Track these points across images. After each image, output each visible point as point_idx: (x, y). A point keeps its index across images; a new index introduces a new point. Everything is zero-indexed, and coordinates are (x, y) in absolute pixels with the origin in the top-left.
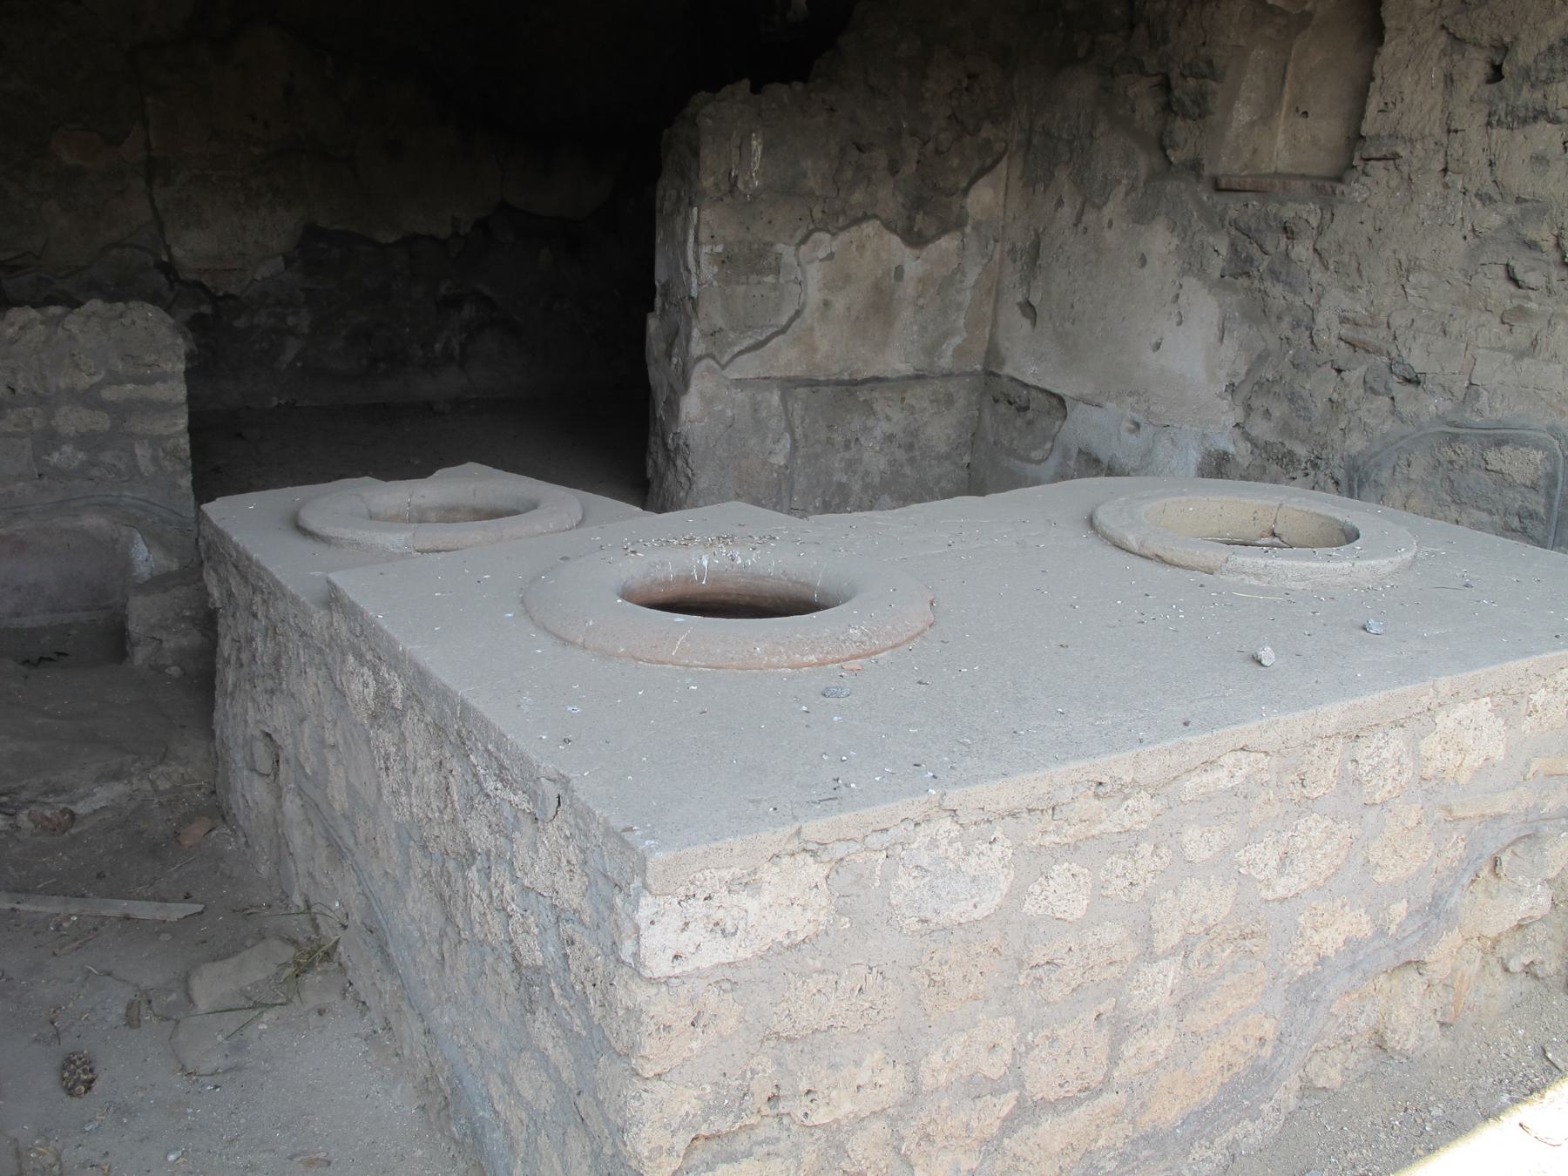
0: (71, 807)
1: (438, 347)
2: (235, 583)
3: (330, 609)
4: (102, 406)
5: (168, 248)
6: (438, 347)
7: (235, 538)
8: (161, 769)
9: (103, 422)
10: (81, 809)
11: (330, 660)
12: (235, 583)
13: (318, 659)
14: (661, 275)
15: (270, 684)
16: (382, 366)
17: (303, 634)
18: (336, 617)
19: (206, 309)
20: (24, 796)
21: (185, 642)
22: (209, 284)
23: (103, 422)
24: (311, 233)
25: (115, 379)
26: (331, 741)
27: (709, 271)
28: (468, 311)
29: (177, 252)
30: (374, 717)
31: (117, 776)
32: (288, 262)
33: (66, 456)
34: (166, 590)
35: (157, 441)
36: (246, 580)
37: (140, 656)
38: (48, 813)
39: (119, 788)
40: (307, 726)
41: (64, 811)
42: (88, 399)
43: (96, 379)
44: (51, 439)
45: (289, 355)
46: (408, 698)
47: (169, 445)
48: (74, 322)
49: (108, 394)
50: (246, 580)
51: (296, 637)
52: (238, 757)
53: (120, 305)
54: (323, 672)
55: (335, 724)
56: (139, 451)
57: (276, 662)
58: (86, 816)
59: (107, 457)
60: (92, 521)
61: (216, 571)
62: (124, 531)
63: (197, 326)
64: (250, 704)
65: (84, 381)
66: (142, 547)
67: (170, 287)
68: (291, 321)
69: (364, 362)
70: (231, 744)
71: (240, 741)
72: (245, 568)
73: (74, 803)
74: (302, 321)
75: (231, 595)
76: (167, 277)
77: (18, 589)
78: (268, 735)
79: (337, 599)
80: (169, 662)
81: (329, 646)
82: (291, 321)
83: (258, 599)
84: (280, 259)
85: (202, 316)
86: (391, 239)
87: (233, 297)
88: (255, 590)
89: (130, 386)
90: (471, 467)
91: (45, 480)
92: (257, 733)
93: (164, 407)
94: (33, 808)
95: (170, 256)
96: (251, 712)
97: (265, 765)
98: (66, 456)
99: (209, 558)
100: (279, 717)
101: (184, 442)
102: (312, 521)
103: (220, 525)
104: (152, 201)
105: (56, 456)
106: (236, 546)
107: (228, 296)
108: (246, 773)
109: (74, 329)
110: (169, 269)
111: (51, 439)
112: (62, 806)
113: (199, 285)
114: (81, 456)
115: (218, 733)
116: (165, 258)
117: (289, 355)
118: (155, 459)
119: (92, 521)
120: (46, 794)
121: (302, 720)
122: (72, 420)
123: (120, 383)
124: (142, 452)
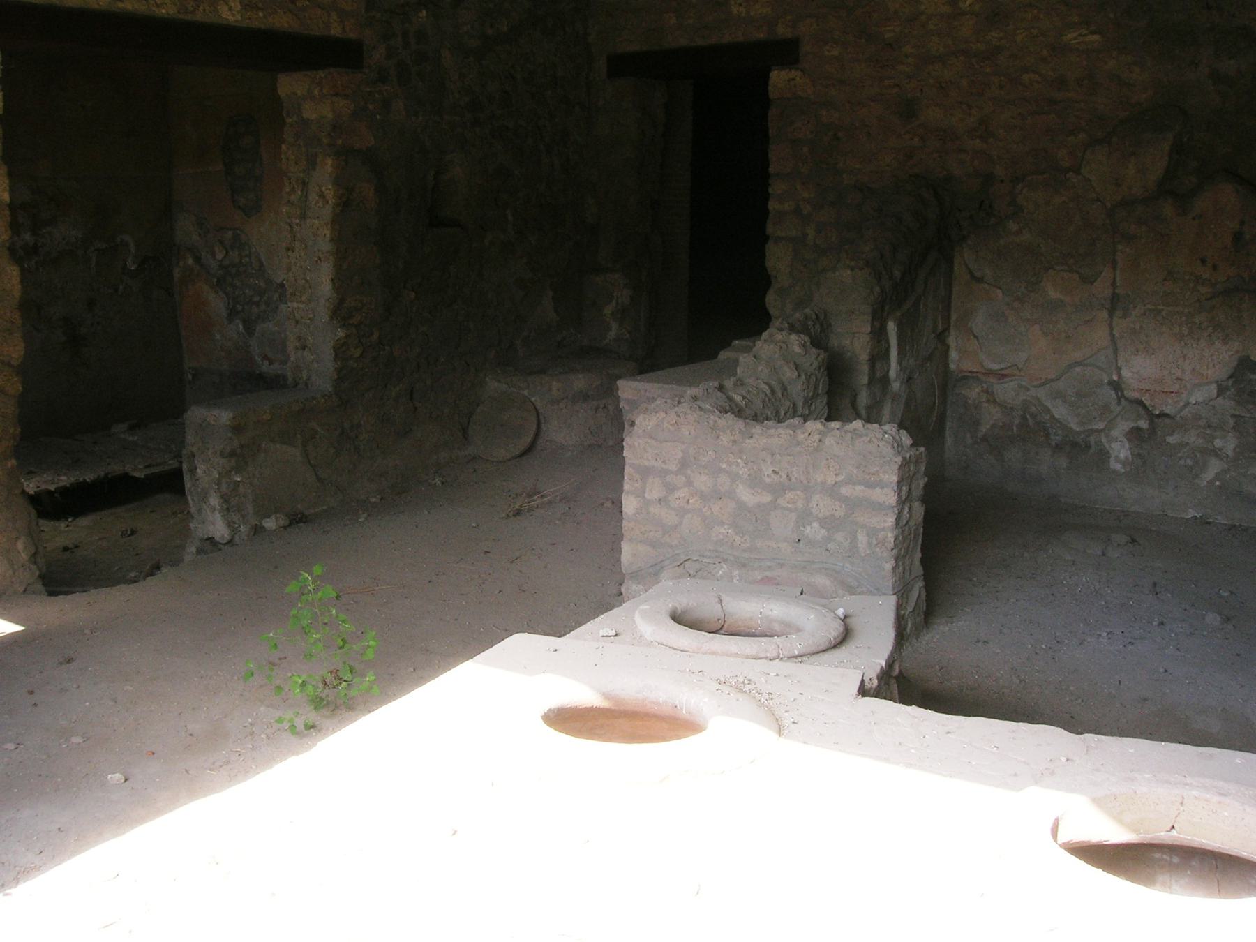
5: (1119, 369)
14: (919, 510)
19: (1143, 424)
22: (1147, 403)
23: (840, 511)
24: (1245, 365)
25: (850, 481)
27: (193, 549)
29: (1126, 373)
32: (1221, 391)
35: (872, 532)
42: (832, 491)
43: (840, 478)
44: (805, 517)
45: (1210, 473)
49: (845, 491)
59: (839, 537)
74: (1228, 444)
82: (1218, 443)
85: (1138, 429)
87: (1167, 416)
89: (859, 488)
93: (878, 507)
95: (1119, 376)
104: (1111, 328)
105: (809, 528)
107: (1163, 415)
110: (1117, 386)
113: (1140, 403)
114: (824, 532)
116: (1115, 378)
117: (1210, 473)
122: (822, 505)
124: (862, 537)
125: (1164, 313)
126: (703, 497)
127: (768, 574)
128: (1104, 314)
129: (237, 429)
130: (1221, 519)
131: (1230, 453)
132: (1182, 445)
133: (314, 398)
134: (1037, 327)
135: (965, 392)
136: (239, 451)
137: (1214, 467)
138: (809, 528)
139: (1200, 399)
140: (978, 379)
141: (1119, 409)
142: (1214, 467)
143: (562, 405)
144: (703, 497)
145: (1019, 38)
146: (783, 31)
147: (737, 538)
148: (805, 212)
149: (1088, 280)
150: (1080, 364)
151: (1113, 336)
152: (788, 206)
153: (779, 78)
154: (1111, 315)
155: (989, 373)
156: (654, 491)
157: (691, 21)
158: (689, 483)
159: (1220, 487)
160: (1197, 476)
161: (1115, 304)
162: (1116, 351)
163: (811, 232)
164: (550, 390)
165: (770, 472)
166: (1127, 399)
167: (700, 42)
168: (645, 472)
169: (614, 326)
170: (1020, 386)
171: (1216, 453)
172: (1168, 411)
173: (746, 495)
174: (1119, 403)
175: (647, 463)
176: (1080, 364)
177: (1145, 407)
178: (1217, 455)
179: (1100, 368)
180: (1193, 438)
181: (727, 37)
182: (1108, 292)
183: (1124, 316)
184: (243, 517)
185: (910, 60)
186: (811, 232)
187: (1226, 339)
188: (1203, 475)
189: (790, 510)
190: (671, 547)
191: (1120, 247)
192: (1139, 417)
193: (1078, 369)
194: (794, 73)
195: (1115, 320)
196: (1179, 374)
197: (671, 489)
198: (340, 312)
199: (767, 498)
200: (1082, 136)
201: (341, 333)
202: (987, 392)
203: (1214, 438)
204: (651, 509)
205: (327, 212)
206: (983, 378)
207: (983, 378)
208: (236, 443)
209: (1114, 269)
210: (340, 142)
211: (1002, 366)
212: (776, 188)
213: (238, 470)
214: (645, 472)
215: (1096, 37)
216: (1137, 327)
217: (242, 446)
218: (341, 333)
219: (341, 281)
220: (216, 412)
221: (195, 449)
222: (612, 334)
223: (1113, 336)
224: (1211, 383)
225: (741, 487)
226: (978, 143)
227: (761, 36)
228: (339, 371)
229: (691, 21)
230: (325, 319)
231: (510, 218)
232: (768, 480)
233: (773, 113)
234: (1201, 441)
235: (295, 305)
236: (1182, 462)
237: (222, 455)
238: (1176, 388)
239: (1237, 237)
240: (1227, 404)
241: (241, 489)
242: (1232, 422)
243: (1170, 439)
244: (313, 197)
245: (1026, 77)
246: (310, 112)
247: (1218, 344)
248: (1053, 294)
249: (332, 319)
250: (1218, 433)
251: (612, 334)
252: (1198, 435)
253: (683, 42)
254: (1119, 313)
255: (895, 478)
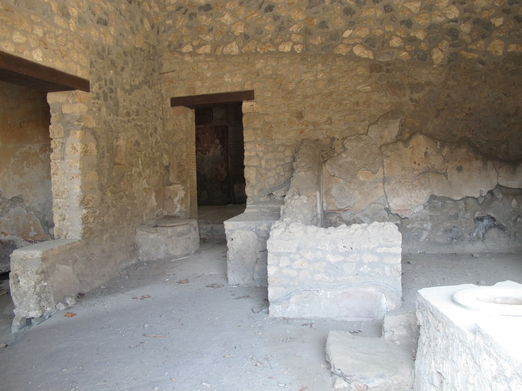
0: (367, 384)
1: (474, 234)
2: (430, 318)
3: (475, 334)
4: (377, 254)
5: (388, 204)
6: (474, 234)
7: (432, 303)
8: (395, 376)
9: (376, 259)
10: (370, 385)
11: (473, 352)
12: (430, 318)
13: (467, 351)
15: (443, 355)
16: (455, 240)
17: (461, 341)
18: (478, 338)
20: (354, 378)
21: (401, 333)
22: (400, 214)
23: (376, 259)
24: (433, 197)
25: (381, 246)
26: (472, 382)
28: (486, 222)
29: (391, 205)
30: (495, 378)
31: (382, 376)
32: (425, 207)
33: (365, 269)
34: (396, 315)
36: (436, 318)
37: (387, 336)
38: (360, 385)
39: (382, 381)
40: (459, 374)
41: (365, 385)
42: (372, 252)
43: (375, 246)
44: (361, 263)
45: (424, 237)
46: (514, 374)
47: (395, 267)
48: (370, 228)
49: (379, 250)
50: (436, 318)
51: (458, 341)
52: (426, 378)
53: (383, 223)
54: (470, 356)
55: (474, 376)
56: (386, 269)
57: (447, 349)
58: (371, 388)
59: (376, 270)
60: (371, 290)
61: (422, 313)
62: (380, 293)
63: (401, 228)
64: (433, 361)
65: (372, 246)
66: (384, 299)
67: (390, 215)
68: (425, 226)
69: (449, 239)
70: (423, 373)
71: (427, 373)
72: (435, 313)
73: (368, 383)
74: (428, 226)
75: (428, 321)
76: (387, 212)
77: (347, 309)
78: (439, 373)
79: (479, 331)
80: (396, 339)
81: (474, 347)
82: (425, 226)
83: (440, 325)
84: (422, 206)
86: (459, 199)
87: (407, 218)
88: (439, 322)
89: (385, 248)
90: (508, 282)
91: (358, 276)
92: (435, 371)
93: (394, 255)
94: (356, 382)
95: (389, 206)
96: (433, 364)
97: (437, 383)
98: (365, 269)
99: (419, 308)
100: (446, 368)
101: (400, 266)
102: (458, 298)
103: (426, 298)
105: (362, 268)
106: (433, 306)
108: (428, 384)
109: (370, 230)
110: (388, 210)
111: (361, 263)
112: (365, 383)
114: (369, 269)
115: (416, 368)
116: (387, 207)
117: (424, 237)
118: (391, 271)
119: (371, 290)
120: (360, 378)
121: (457, 372)
122: (367, 258)
123: (382, 247)
125: (403, 182)
126: (309, 262)
127: (345, 291)
128: (381, 184)
129: (44, 259)
130: (429, 252)
131: (430, 229)
132: (413, 228)
133: (75, 243)
134: (356, 191)
135: (330, 218)
136: (46, 270)
137: (425, 234)
138: (362, 268)
139: (418, 211)
140: (336, 213)
141: (389, 218)
142: (425, 234)
143: (173, 238)
144: (309, 262)
145: (341, 88)
146: (247, 88)
147: (327, 278)
148: (260, 156)
149: (374, 173)
150: (374, 203)
151: (385, 192)
152: (253, 154)
153: (246, 106)
154: (384, 184)
155: (340, 210)
156: (284, 262)
157: (207, 84)
158: (302, 257)
159: (428, 241)
160: (419, 238)
161: (385, 180)
162: (387, 197)
163: (263, 163)
164: (167, 232)
165: (342, 247)
166: (392, 214)
167: (211, 92)
168: (279, 255)
169: (179, 206)
170: (352, 214)
171: (425, 229)
172: (407, 217)
173: (331, 259)
174: (389, 216)
175: (280, 251)
176: (374, 203)
177: (399, 216)
178: (425, 230)
179: (381, 204)
180: (416, 225)
181: (223, 90)
182: (382, 176)
183: (388, 185)
184: (49, 303)
185: (299, 97)
186: (263, 163)
187: (425, 189)
188: (422, 238)
189: (353, 262)
190: (294, 286)
191: (385, 160)
192: (397, 220)
193: (373, 205)
194: (252, 103)
195: (385, 186)
196: (410, 203)
197: (293, 261)
198: (84, 203)
199: (342, 258)
200: (367, 122)
201: (85, 211)
202: (339, 217)
203: (423, 224)
204: (283, 271)
205: (78, 155)
206: (337, 212)
207: (337, 212)
208: (44, 266)
209: (383, 168)
210: (82, 124)
211: (344, 207)
212: (247, 147)
213: (45, 280)
214: (279, 255)
215: (369, 87)
216: (394, 187)
217: (47, 268)
218: (85, 211)
219: (84, 186)
220: (32, 252)
221: (18, 272)
222: (178, 209)
223: (385, 192)
224: (420, 205)
225: (328, 255)
226: (328, 126)
227: (238, 89)
228: (84, 229)
229: (207, 84)
230: (77, 205)
231: (140, 162)
232: (341, 251)
233: (244, 119)
234: (419, 226)
235: (58, 200)
236: (414, 234)
237: (37, 273)
238: (409, 208)
239: (426, 153)
240: (427, 212)
241: (47, 289)
242: (429, 218)
243: (408, 227)
244: (68, 149)
245: (344, 102)
246: (66, 110)
247: (423, 191)
248: (362, 179)
249: (80, 205)
250: (424, 222)
251: (178, 209)
252: (418, 224)
253: (204, 92)
254: (386, 184)
255: (401, 242)
